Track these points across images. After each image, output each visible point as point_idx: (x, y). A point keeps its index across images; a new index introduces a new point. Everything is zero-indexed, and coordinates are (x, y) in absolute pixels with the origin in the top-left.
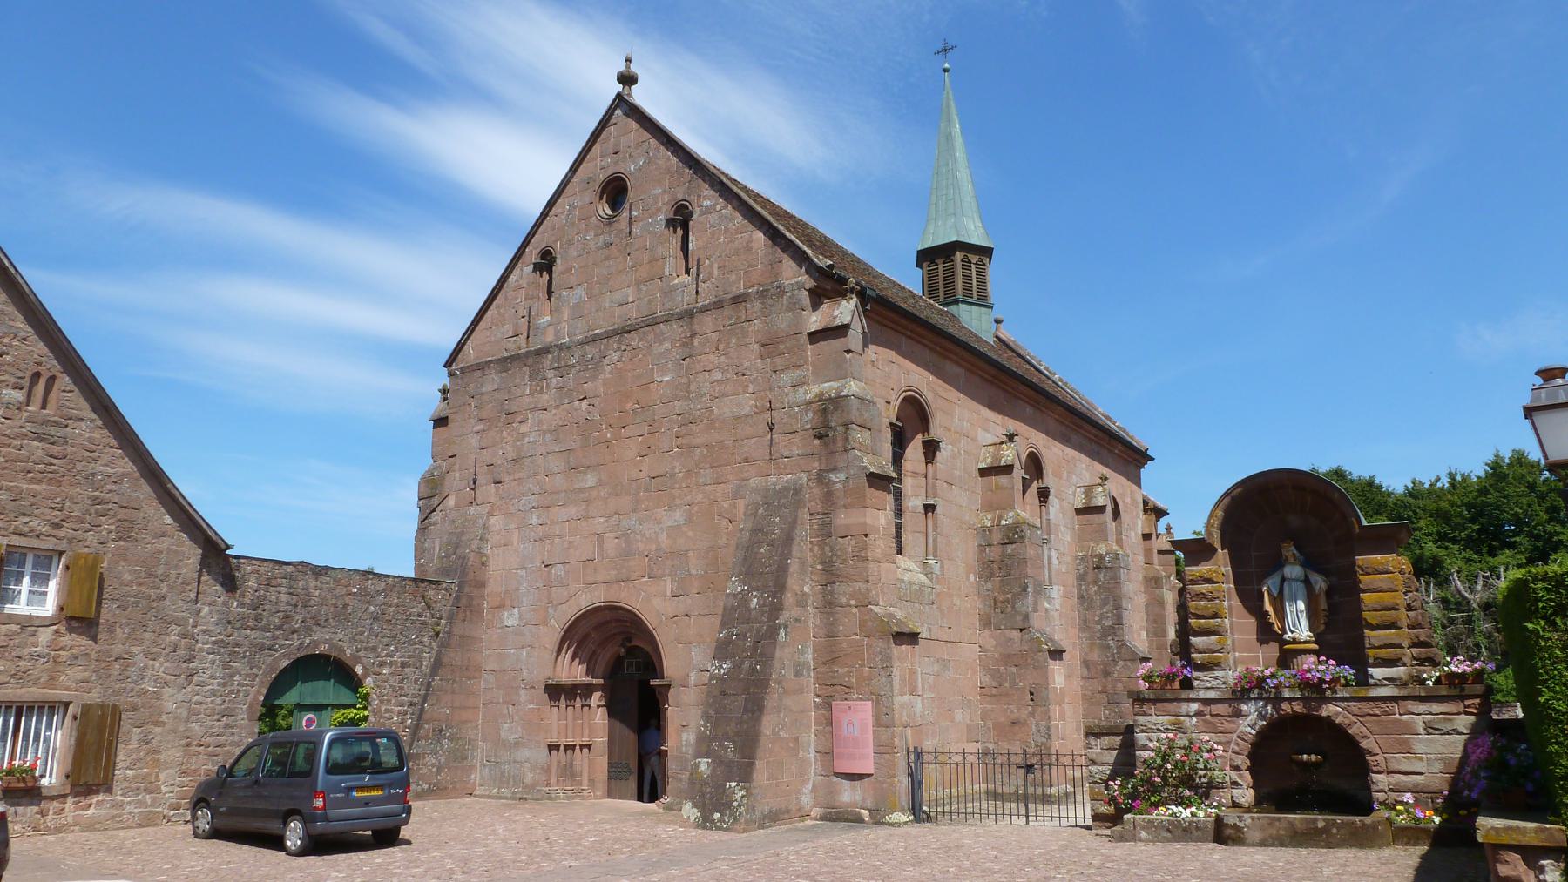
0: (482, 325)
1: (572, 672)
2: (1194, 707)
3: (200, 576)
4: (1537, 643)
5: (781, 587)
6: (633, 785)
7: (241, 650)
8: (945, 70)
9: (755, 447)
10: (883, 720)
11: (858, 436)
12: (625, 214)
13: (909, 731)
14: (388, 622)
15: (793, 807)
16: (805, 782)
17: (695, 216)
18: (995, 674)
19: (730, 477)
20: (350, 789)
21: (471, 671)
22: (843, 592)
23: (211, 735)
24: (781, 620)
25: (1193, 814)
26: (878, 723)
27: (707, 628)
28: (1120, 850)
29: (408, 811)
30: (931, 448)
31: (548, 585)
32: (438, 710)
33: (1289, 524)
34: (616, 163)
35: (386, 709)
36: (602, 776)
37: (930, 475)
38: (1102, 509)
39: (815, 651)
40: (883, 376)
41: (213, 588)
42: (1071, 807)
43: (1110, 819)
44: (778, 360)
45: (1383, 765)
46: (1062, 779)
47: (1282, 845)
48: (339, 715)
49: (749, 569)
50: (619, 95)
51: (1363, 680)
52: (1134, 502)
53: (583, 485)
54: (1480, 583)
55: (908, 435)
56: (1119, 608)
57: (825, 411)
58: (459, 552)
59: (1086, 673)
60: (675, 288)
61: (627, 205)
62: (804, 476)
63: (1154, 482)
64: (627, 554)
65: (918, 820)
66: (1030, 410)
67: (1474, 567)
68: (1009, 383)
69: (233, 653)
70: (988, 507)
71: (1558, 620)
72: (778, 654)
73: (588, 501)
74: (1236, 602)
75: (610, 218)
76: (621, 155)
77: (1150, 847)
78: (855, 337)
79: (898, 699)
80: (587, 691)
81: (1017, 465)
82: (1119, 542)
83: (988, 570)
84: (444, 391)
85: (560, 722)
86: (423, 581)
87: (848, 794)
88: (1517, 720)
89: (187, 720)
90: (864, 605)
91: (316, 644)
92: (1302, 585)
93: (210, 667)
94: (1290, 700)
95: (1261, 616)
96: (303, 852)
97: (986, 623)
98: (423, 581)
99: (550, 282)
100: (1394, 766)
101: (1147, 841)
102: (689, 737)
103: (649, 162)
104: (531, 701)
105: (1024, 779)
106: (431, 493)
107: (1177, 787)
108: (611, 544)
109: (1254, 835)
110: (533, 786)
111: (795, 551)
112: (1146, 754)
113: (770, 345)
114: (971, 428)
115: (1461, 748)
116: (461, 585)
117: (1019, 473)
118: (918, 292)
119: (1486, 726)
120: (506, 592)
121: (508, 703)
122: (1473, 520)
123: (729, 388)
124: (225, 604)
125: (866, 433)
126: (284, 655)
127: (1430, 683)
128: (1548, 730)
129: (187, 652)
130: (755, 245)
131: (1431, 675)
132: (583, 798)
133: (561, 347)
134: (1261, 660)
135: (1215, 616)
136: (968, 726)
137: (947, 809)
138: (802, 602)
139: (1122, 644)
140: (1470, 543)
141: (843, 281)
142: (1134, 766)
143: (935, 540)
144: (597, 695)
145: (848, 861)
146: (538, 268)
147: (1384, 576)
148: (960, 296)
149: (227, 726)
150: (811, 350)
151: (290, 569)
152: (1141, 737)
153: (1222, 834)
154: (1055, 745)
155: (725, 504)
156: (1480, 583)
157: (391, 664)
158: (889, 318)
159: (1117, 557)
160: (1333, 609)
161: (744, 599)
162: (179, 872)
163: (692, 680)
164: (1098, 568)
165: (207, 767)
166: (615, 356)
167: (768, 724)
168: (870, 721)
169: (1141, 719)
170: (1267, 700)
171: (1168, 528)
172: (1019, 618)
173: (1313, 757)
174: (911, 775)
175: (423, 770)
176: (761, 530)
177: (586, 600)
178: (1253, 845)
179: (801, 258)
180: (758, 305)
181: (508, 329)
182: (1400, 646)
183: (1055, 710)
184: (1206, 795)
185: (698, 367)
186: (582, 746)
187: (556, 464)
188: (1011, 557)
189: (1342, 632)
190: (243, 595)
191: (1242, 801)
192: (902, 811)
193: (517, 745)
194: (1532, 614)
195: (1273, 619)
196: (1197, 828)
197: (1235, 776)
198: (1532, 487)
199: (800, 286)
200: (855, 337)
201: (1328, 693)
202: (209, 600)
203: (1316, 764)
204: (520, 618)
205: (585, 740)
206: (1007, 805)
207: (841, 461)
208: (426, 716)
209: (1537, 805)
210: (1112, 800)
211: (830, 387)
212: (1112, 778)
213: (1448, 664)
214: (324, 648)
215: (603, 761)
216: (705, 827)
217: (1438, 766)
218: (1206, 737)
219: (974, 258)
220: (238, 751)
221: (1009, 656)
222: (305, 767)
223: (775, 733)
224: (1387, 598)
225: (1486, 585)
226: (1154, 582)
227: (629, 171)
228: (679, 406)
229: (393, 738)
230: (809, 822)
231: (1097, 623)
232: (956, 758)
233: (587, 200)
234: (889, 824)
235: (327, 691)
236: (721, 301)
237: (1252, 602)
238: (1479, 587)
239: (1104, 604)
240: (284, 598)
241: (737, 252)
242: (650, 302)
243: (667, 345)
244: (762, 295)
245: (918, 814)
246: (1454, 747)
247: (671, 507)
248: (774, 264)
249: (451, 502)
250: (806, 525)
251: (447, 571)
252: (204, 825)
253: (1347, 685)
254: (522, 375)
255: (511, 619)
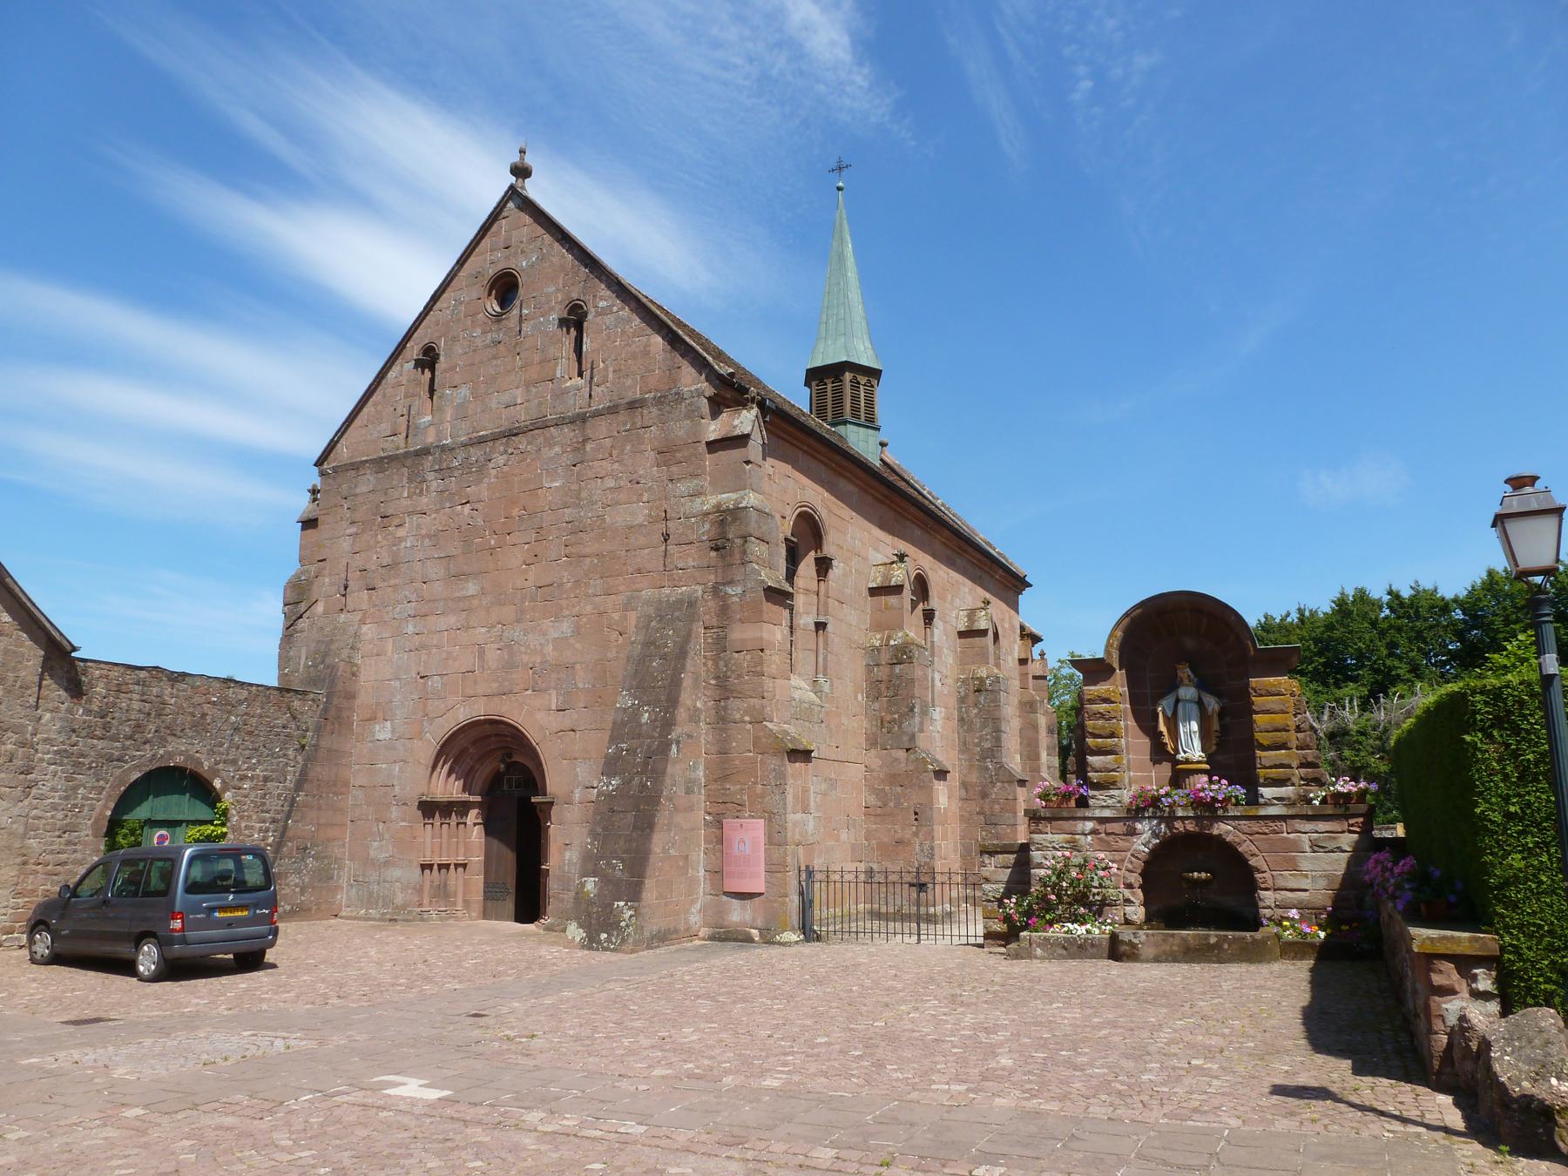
0: (358, 422)
1: (448, 788)
2: (1090, 825)
3: (41, 679)
4: (1474, 755)
5: (673, 702)
6: (510, 905)
7: (86, 761)
8: (839, 189)
9: (649, 557)
10: (776, 838)
11: (756, 549)
12: (515, 312)
13: (801, 850)
14: (250, 733)
15: (682, 927)
16: (693, 902)
17: (590, 317)
18: (880, 794)
19: (621, 588)
20: (212, 909)
21: (339, 786)
22: (737, 708)
23: (52, 852)
24: (673, 736)
25: (1088, 932)
26: (770, 841)
27: (596, 743)
28: (1019, 967)
29: (275, 932)
30: (824, 566)
31: (424, 698)
32: (302, 827)
33: (1179, 643)
34: (507, 258)
35: (246, 822)
36: (478, 895)
37: (822, 593)
38: (984, 633)
39: (706, 768)
40: (780, 490)
41: (55, 692)
42: (955, 926)
43: (1006, 936)
44: (674, 469)
45: (1270, 882)
46: (946, 899)
47: (1175, 960)
48: (194, 832)
49: (640, 683)
50: (512, 187)
51: (1253, 799)
52: (1012, 627)
53: (463, 593)
54: (1327, 711)
55: (801, 550)
56: (998, 730)
57: (722, 523)
58: (328, 661)
59: (963, 793)
60: (566, 391)
61: (517, 302)
62: (699, 588)
63: (1032, 609)
64: (509, 666)
65: (807, 939)
66: (918, 532)
67: (1322, 698)
68: (894, 501)
69: (77, 764)
70: (877, 626)
71: (1495, 733)
72: (669, 769)
73: (470, 610)
74: (1131, 722)
75: (499, 315)
76: (512, 250)
77: (1046, 964)
78: (755, 448)
79: (791, 817)
80: (463, 808)
81: (907, 586)
82: (998, 665)
83: (875, 689)
84: (314, 491)
85: (433, 840)
86: (288, 691)
87: (737, 914)
88: (1397, 839)
89: (24, 836)
90: (758, 721)
91: (170, 755)
92: (1195, 707)
93: (51, 779)
94: (1183, 819)
95: (1155, 736)
96: (157, 978)
97: (872, 743)
98: (288, 691)
99: (432, 380)
100: (1281, 883)
101: (1042, 958)
102: (573, 855)
103: (542, 259)
104: (403, 818)
105: (909, 898)
106: (297, 600)
107: (1071, 904)
108: (493, 655)
109: (1148, 951)
110: (404, 907)
111: (689, 663)
112: (1042, 872)
113: (666, 453)
114: (863, 547)
115: (1344, 865)
116: (329, 696)
117: (907, 594)
118: (806, 410)
119: (1369, 846)
120: (378, 704)
121: (377, 820)
122: (1320, 654)
123: (622, 497)
124: (69, 711)
125: (764, 547)
126: (136, 767)
127: (1317, 802)
128: (1482, 841)
129: (24, 762)
130: (653, 349)
131: (1317, 795)
132: (457, 919)
133: (443, 448)
134: (1154, 779)
135: (1112, 735)
136: (853, 846)
137: (831, 928)
138: (694, 717)
139: (1001, 767)
140: (1316, 676)
141: (747, 391)
142: (1029, 884)
143: (825, 659)
144: (473, 813)
145: (746, 982)
146: (419, 364)
147: (1278, 699)
148: (848, 417)
149: (68, 843)
150: (709, 460)
151: (143, 674)
152: (1036, 855)
153: (1116, 950)
154: (939, 866)
155: (616, 616)
156: (1327, 711)
157: (252, 778)
158: (784, 428)
159: (997, 680)
160: (1224, 729)
161: (635, 713)
162: (16, 1000)
163: (577, 796)
164: (978, 691)
165: (47, 887)
166: (501, 460)
167: (658, 842)
168: (762, 840)
169: (1037, 837)
170: (1161, 819)
171: (1042, 654)
172: (905, 738)
173: (1203, 875)
174: (801, 894)
175: (288, 888)
176: (653, 643)
177: (464, 714)
178: (1147, 961)
179: (701, 365)
180: (655, 411)
181: (386, 428)
182: (1289, 767)
183: (938, 830)
184: (1100, 913)
185: (591, 474)
186: (457, 866)
187: (435, 571)
188: (899, 677)
189: (1234, 753)
190: (90, 701)
191: (1134, 918)
192: (793, 930)
193: (387, 863)
194: (1470, 727)
195: (1166, 739)
196: (1093, 945)
197: (1127, 893)
198: (1374, 624)
199: (700, 393)
200: (755, 448)
201: (1220, 812)
202: (50, 706)
203: (1206, 881)
204: (393, 731)
205: (461, 859)
206: (891, 925)
207: (738, 574)
208: (289, 834)
209: (1470, 915)
210: (1007, 919)
211: (728, 498)
212: (1007, 894)
213: (1334, 784)
214: (179, 760)
215: (479, 880)
216: (590, 948)
217: (1322, 883)
218: (1102, 855)
219: (863, 380)
220: (82, 870)
221: (894, 776)
222: (162, 887)
223: (665, 851)
224: (1278, 720)
225: (1332, 715)
226: (1029, 707)
227: (518, 269)
228: (568, 513)
229: (258, 853)
230: (697, 942)
231: (978, 745)
232: (847, 877)
233: (475, 296)
234: (780, 944)
235: (182, 806)
236: (616, 406)
237: (1147, 723)
238: (1325, 718)
239: (984, 726)
240: (136, 705)
241: (634, 356)
242: (540, 404)
243: (557, 449)
244: (659, 401)
245: (809, 933)
246: (1337, 864)
247: (558, 617)
248: (672, 374)
249: (320, 608)
250: (700, 639)
251: (314, 681)
252: (42, 949)
253: (1237, 804)
254: (399, 479)
255: (383, 732)
